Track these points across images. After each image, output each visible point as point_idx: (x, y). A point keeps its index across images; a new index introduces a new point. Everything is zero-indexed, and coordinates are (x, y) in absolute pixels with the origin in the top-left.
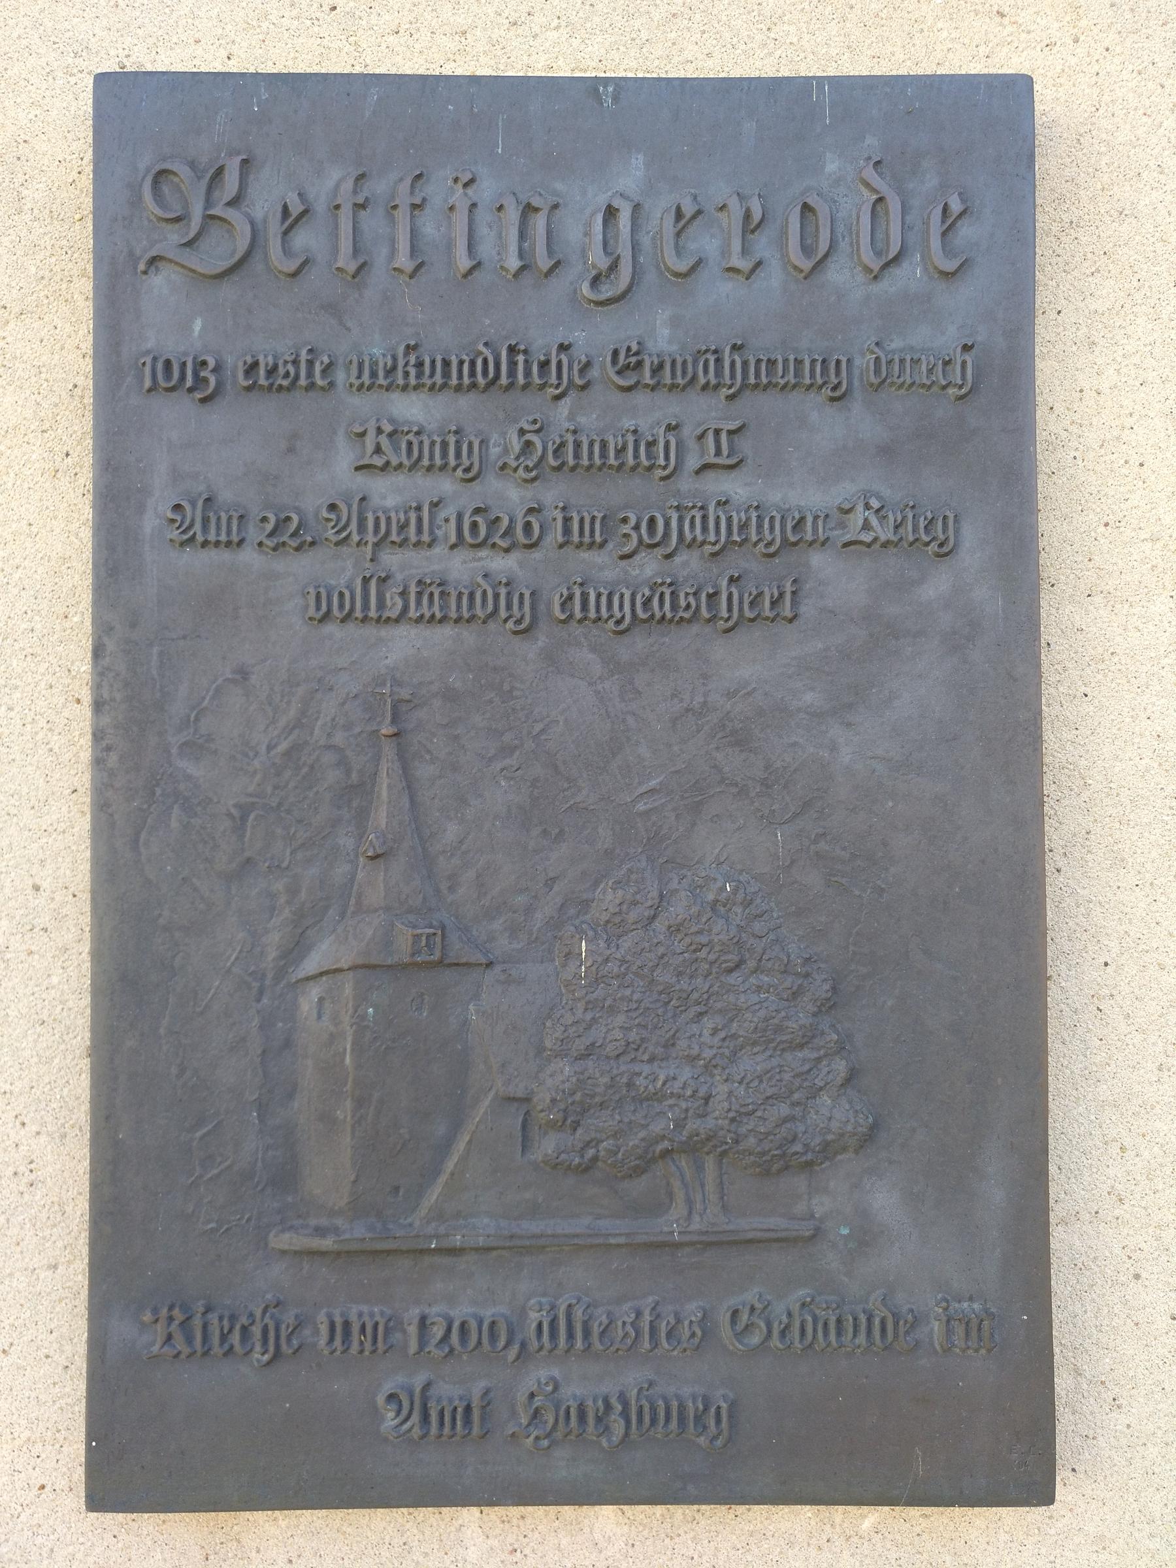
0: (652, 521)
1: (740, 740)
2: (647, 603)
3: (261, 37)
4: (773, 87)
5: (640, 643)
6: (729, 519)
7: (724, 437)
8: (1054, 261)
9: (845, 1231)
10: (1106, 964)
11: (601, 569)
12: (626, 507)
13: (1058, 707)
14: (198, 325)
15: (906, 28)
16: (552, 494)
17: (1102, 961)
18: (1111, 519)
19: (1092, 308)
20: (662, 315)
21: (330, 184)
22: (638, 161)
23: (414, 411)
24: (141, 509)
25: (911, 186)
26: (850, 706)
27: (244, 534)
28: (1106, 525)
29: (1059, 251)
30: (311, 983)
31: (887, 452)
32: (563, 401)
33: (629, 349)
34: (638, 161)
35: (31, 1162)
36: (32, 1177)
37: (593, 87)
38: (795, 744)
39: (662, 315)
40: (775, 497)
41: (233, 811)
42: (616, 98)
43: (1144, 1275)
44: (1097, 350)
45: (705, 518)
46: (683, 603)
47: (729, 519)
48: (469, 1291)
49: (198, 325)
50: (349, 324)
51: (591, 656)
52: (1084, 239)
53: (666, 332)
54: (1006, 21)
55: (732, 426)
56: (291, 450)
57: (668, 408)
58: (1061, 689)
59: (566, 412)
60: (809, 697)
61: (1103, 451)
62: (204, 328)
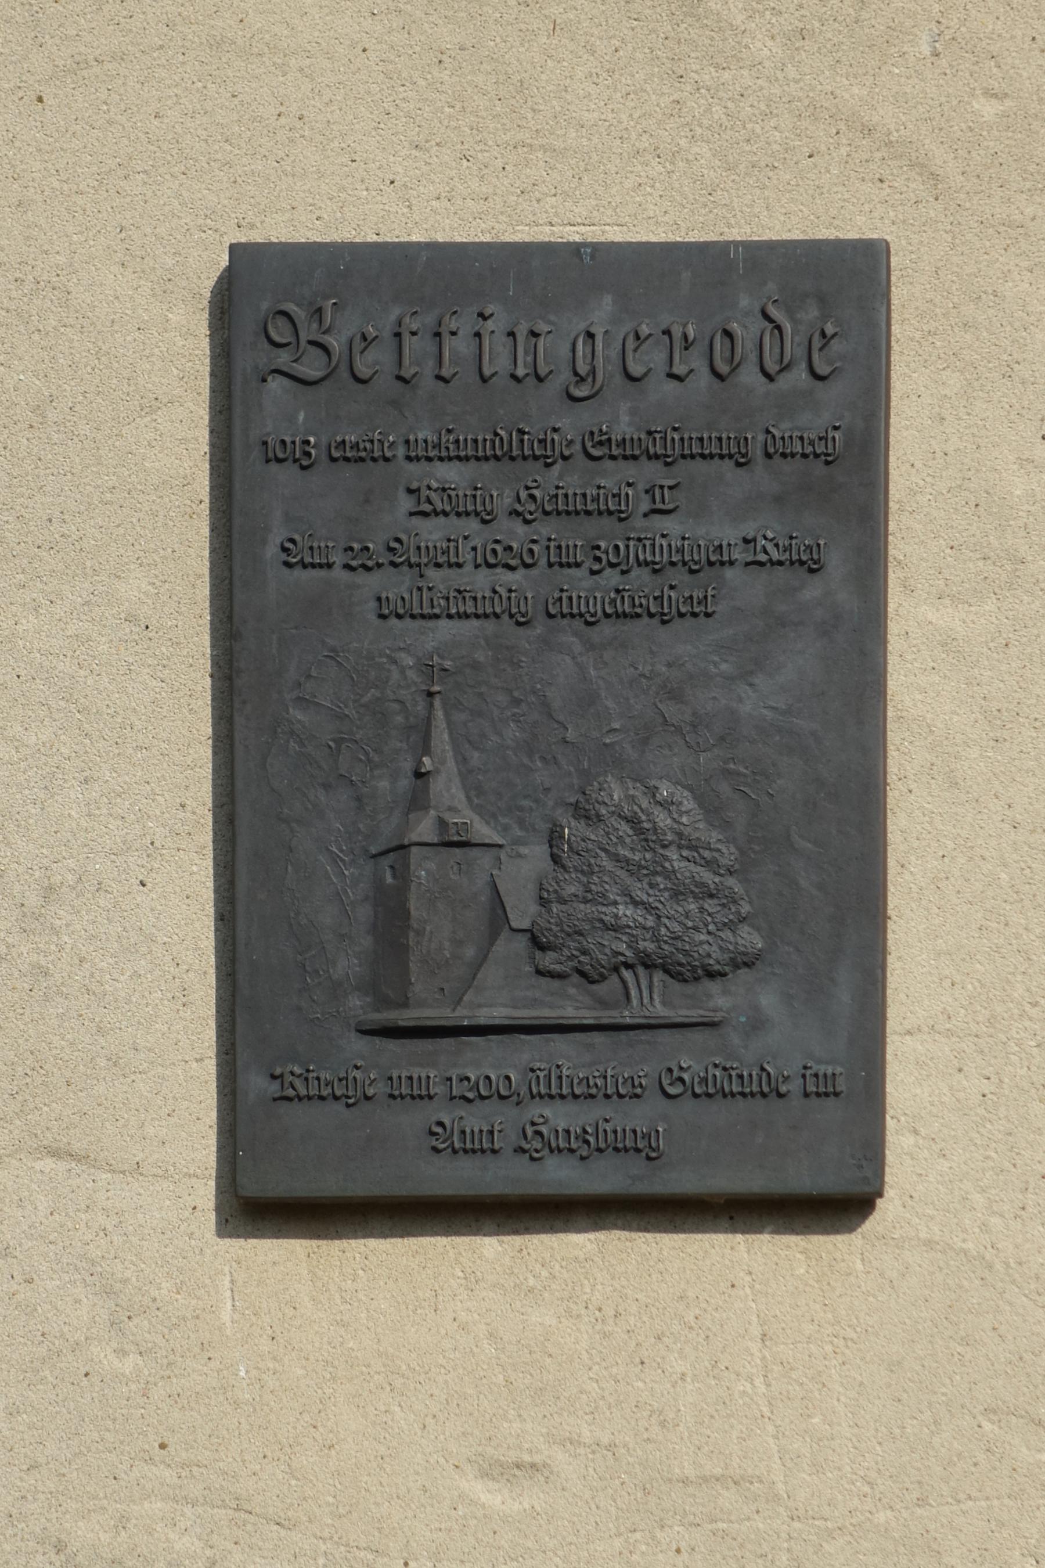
0: (617, 547)
1: (675, 695)
2: (613, 602)
3: (340, 204)
4: (702, 249)
5: (607, 629)
6: (670, 546)
7: (666, 490)
8: (916, 359)
9: (743, 1019)
10: (944, 856)
11: (580, 580)
12: (599, 538)
13: (913, 677)
14: (301, 417)
15: (810, 192)
16: (545, 529)
17: (941, 854)
18: (955, 543)
19: (943, 393)
20: (624, 407)
21: (393, 317)
22: (608, 299)
23: (452, 474)
24: (264, 542)
25: (799, 316)
26: (752, 672)
27: (698, 458)
28: (952, 548)
29: (921, 352)
30: (383, 857)
31: (779, 500)
32: (554, 467)
33: (601, 430)
34: (608, 299)
35: (185, 990)
36: (184, 1000)
37: (576, 249)
38: (714, 698)
39: (624, 407)
40: (701, 531)
41: (331, 743)
42: (593, 257)
43: (965, 1069)
44: (946, 423)
45: (653, 545)
46: (637, 602)
47: (670, 546)
48: (490, 1058)
49: (301, 417)
50: (406, 414)
51: (575, 639)
52: (938, 344)
53: (627, 419)
54: (885, 185)
55: (671, 483)
56: (367, 501)
57: (629, 471)
58: (916, 664)
59: (556, 474)
60: (724, 667)
61: (949, 495)
62: (305, 419)
